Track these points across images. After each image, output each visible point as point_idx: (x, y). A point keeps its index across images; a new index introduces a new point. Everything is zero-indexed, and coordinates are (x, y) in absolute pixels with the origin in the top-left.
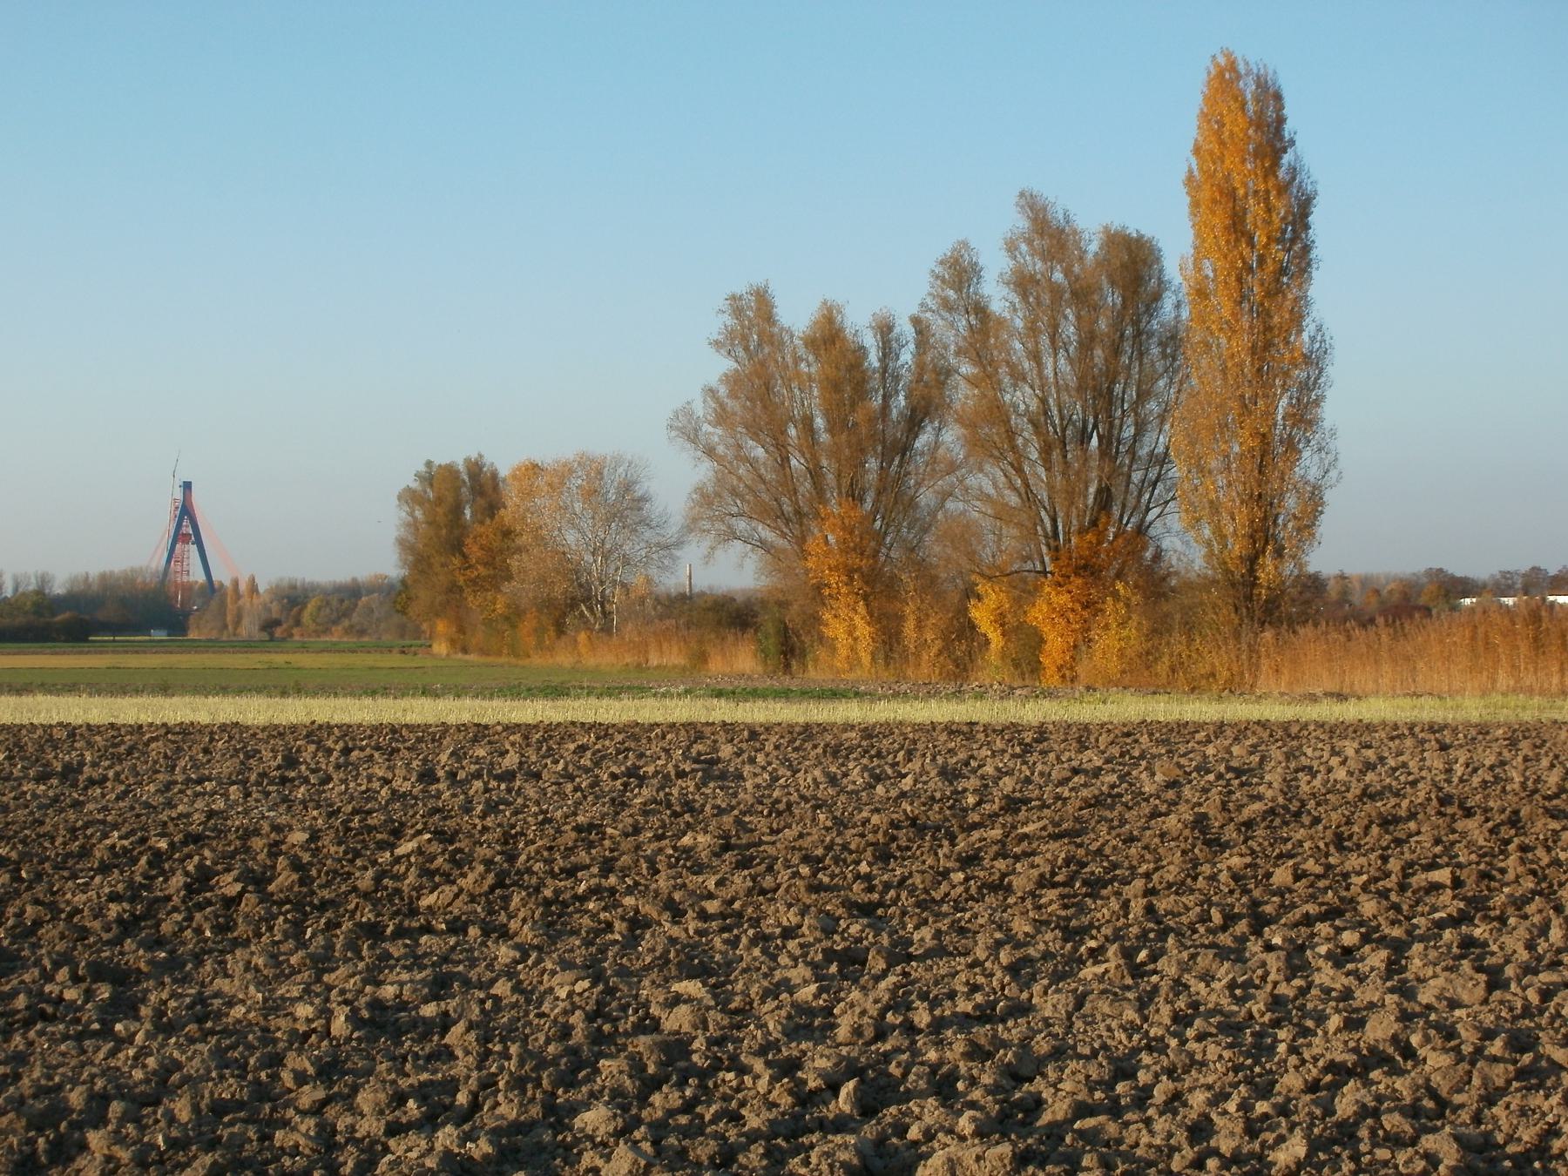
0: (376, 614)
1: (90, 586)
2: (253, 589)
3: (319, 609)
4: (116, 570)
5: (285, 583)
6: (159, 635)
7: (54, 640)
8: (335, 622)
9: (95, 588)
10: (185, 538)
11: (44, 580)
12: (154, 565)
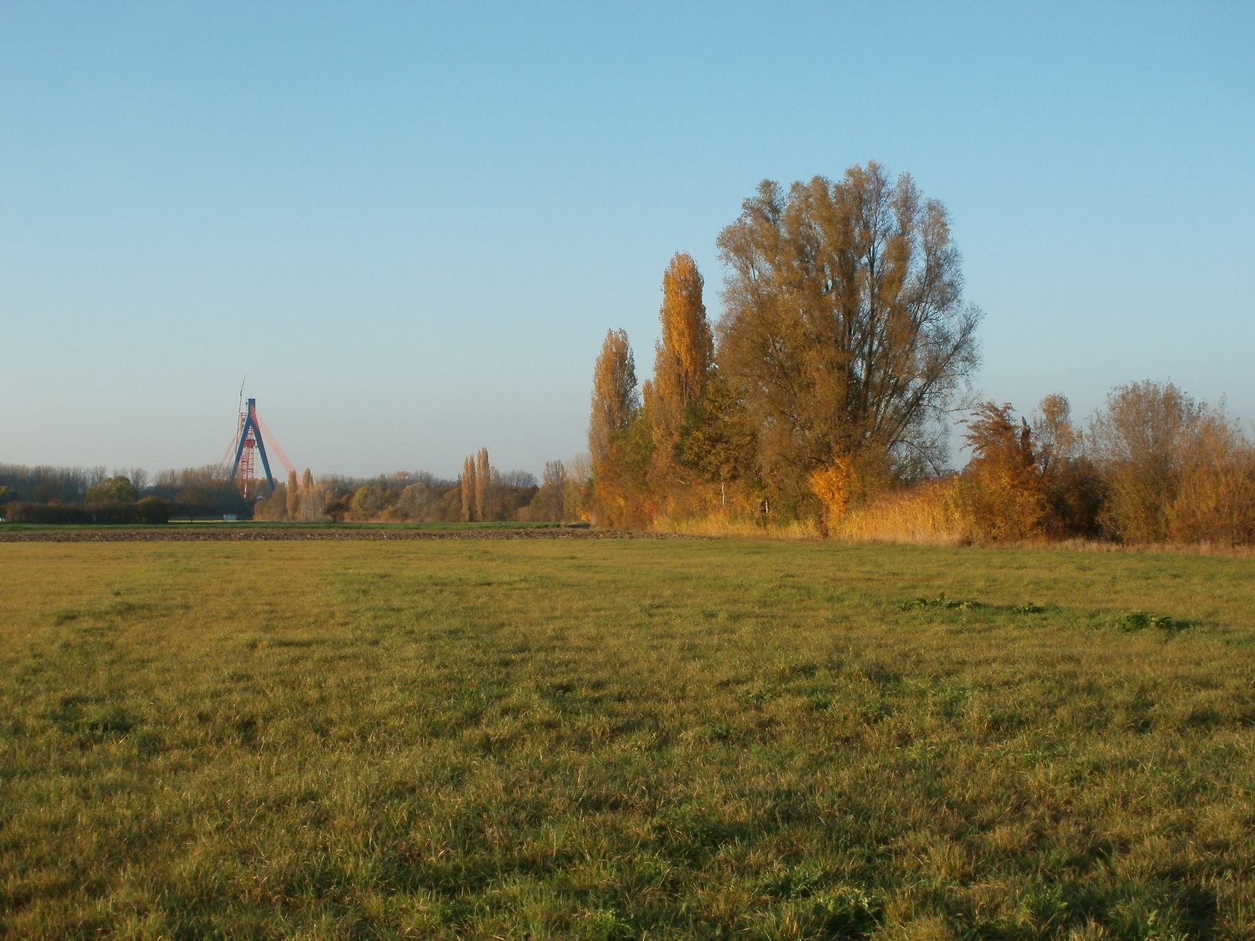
0: (418, 501)
1: (175, 480)
2: (308, 477)
3: (366, 496)
4: (196, 468)
5: (329, 478)
6: (231, 519)
7: (136, 522)
8: (381, 507)
9: (179, 482)
10: (250, 444)
11: (138, 475)
12: (226, 464)
